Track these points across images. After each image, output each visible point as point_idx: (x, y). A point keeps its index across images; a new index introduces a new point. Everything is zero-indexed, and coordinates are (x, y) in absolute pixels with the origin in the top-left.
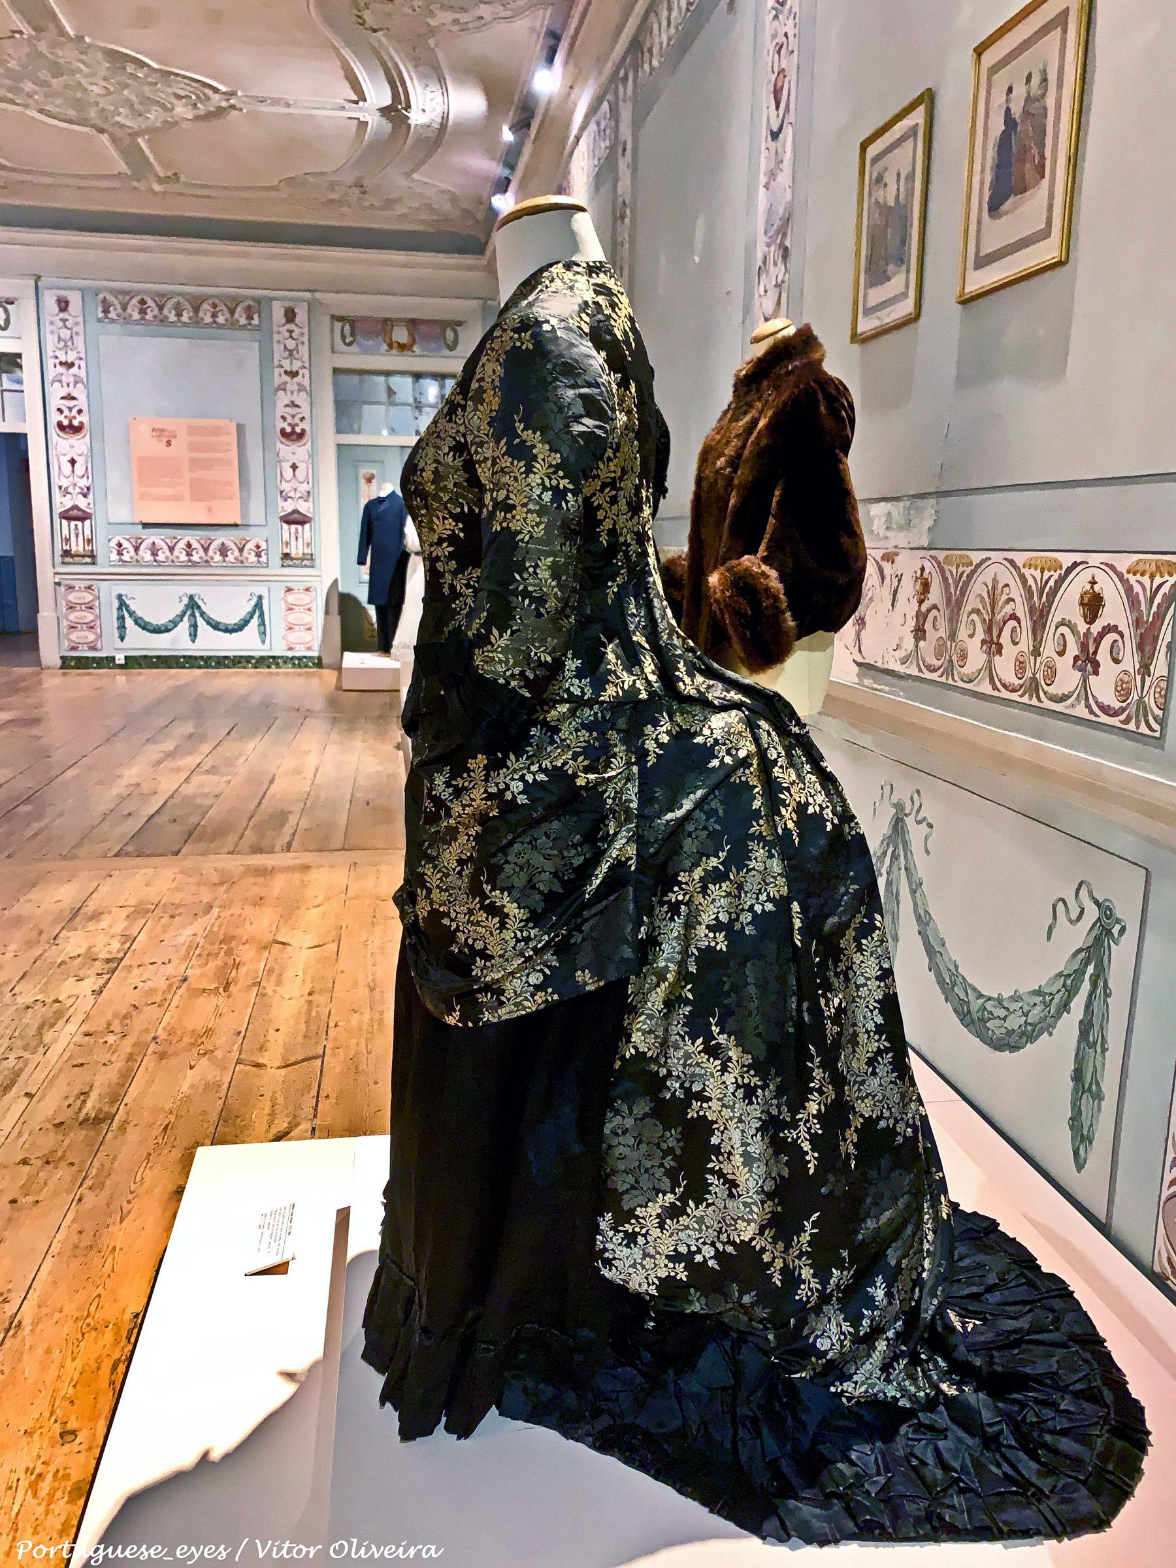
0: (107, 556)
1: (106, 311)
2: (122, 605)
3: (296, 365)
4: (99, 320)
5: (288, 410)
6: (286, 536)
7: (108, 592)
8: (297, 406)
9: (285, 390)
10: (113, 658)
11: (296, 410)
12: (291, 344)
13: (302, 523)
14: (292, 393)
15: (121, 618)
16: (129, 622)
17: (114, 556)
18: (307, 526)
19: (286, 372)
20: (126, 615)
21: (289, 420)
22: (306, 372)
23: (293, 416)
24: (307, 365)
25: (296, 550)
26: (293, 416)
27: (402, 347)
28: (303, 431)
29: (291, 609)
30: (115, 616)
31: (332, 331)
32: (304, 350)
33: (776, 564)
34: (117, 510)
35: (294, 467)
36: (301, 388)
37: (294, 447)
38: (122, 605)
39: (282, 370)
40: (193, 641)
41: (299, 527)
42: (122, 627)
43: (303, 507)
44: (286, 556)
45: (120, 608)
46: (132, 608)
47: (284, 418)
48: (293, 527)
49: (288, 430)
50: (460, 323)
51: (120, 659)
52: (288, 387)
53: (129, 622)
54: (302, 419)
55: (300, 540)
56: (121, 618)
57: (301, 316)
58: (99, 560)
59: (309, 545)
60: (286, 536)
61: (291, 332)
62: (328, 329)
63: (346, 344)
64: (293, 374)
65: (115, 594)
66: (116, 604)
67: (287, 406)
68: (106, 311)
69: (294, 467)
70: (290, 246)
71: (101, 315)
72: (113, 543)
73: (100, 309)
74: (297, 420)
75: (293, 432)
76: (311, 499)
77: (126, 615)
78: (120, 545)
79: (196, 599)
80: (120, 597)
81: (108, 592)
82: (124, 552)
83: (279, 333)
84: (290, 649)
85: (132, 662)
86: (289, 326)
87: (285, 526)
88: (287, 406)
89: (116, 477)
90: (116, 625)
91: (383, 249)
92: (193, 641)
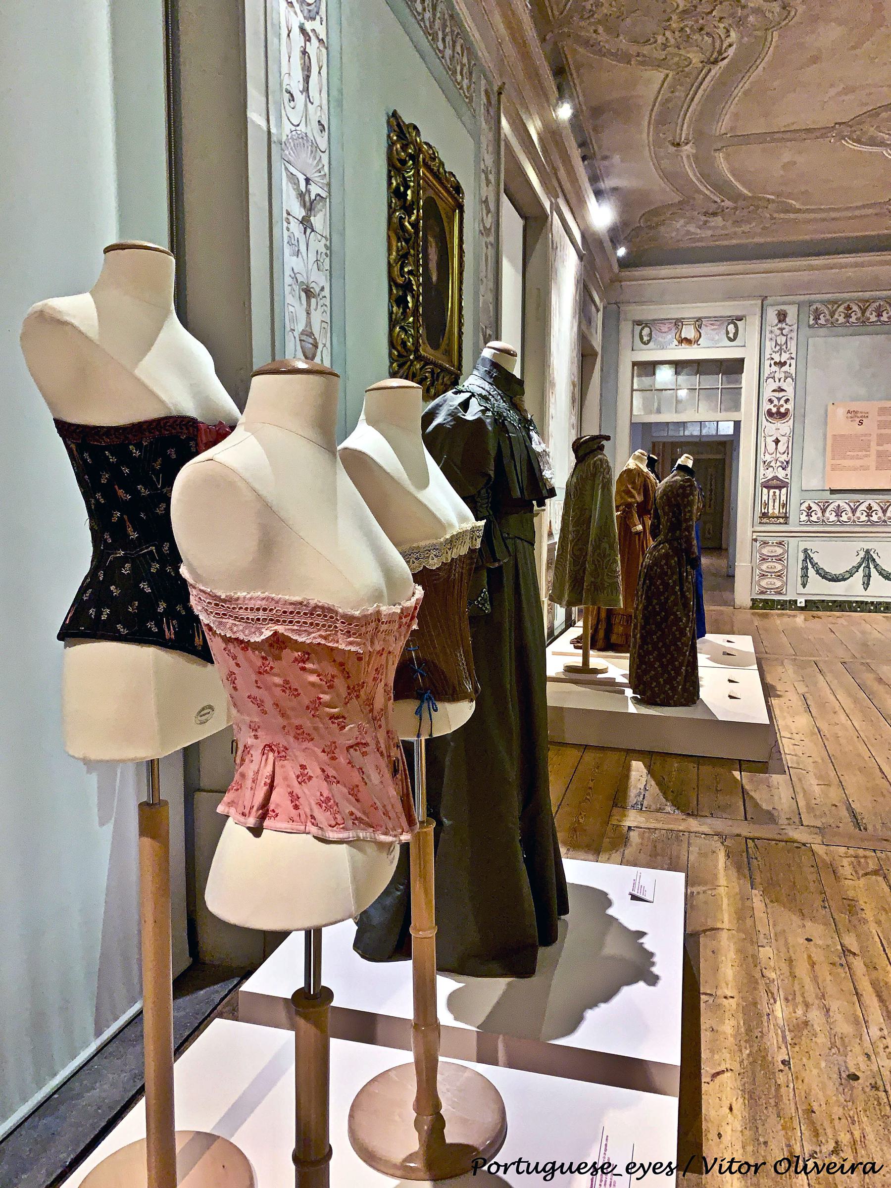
0: (797, 516)
1: (817, 318)
2: (807, 557)
3: (784, 357)
4: (810, 326)
5: (777, 394)
6: (765, 498)
7: (796, 547)
8: (783, 390)
9: (773, 378)
10: (796, 601)
11: (781, 394)
12: (782, 340)
13: (780, 488)
14: (780, 380)
15: (805, 569)
16: (811, 572)
17: (804, 517)
18: (784, 490)
19: (775, 363)
20: (810, 566)
21: (776, 402)
22: (793, 362)
23: (779, 399)
24: (794, 356)
25: (774, 509)
26: (779, 399)
27: (688, 341)
28: (787, 410)
29: (764, 559)
30: (800, 566)
31: (633, 331)
32: (792, 345)
33: (160, 511)
34: (810, 478)
35: (777, 442)
36: (787, 376)
37: (779, 424)
38: (807, 557)
39: (772, 362)
40: (804, 587)
41: (777, 491)
42: (805, 576)
43: (781, 474)
44: (764, 515)
45: (805, 560)
46: (816, 560)
47: (771, 401)
48: (772, 491)
49: (774, 410)
50: (740, 319)
51: (801, 602)
52: (777, 376)
53: (811, 572)
54: (787, 401)
55: (777, 504)
56: (805, 569)
57: (791, 318)
58: (791, 520)
59: (784, 505)
60: (765, 498)
61: (781, 329)
62: (630, 330)
63: (645, 343)
64: (781, 364)
65: (802, 548)
66: (802, 556)
67: (774, 391)
68: (817, 318)
69: (777, 442)
70: (685, 266)
71: (812, 322)
72: (804, 507)
73: (812, 317)
74: (782, 402)
75: (778, 412)
76: (789, 468)
77: (810, 566)
78: (810, 508)
79: (809, 552)
80: (805, 551)
81: (796, 547)
82: (813, 514)
83: (771, 332)
84: (762, 593)
85: (811, 606)
86: (780, 326)
87: (765, 490)
88: (774, 391)
89: (811, 450)
90: (800, 573)
91: (692, 263)
92: (804, 587)
